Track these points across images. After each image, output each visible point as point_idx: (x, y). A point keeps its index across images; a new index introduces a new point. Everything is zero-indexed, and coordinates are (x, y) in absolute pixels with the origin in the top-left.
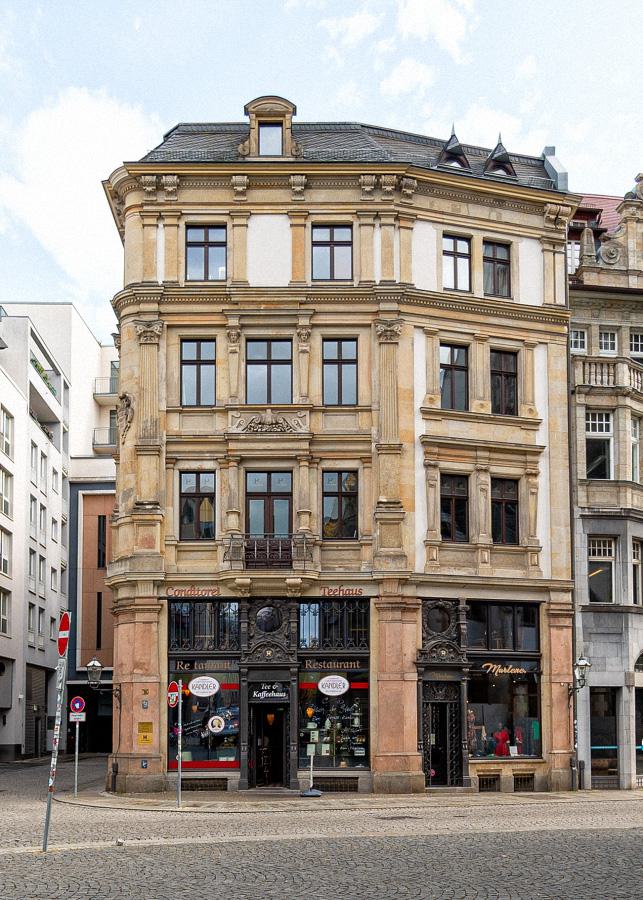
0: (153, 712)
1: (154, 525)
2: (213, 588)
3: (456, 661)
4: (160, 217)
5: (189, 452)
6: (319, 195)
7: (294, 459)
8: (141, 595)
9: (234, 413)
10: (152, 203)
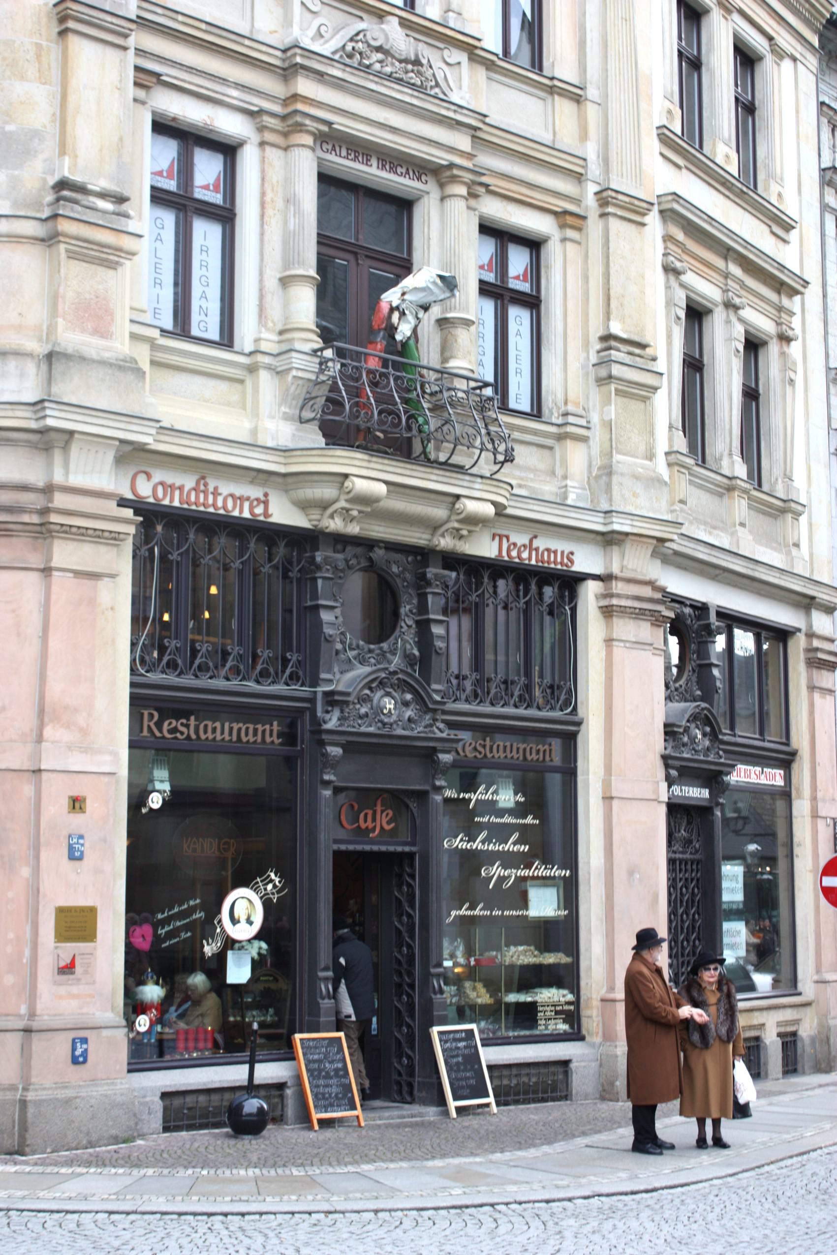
0: (98, 871)
1: (112, 266)
2: (255, 492)
3: (418, 730)
5: (190, 69)
8: (76, 480)
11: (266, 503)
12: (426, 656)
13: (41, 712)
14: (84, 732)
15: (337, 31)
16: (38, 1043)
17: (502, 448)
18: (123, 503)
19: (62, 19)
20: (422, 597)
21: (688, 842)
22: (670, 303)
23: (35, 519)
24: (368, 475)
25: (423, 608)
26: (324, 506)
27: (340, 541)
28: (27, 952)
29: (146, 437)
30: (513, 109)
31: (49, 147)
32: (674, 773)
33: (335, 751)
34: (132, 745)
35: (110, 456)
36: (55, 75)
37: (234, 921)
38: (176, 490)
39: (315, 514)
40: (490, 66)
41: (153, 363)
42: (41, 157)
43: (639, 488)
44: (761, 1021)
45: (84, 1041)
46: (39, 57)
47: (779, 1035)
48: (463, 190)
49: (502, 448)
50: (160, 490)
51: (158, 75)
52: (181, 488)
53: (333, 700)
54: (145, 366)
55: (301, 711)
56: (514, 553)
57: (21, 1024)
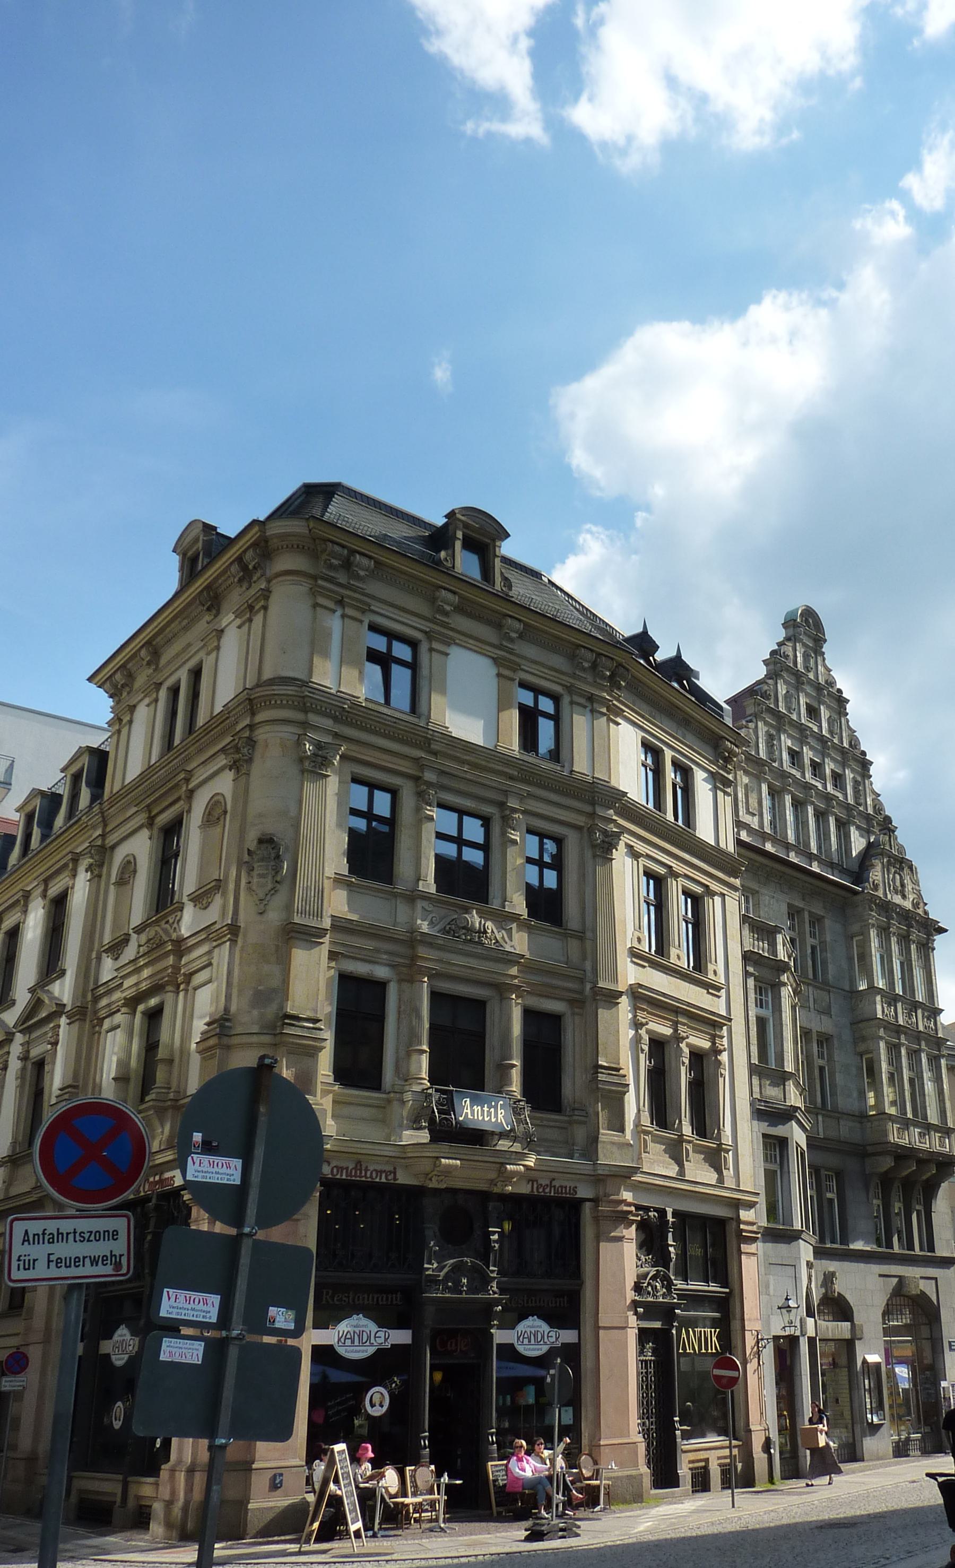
11: (395, 1173)
15: (441, 919)
43: (615, 1149)
44: (706, 1456)
45: (281, 1475)
46: (277, 951)
47: (720, 1465)
50: (335, 1170)
52: (347, 1169)
56: (541, 1190)
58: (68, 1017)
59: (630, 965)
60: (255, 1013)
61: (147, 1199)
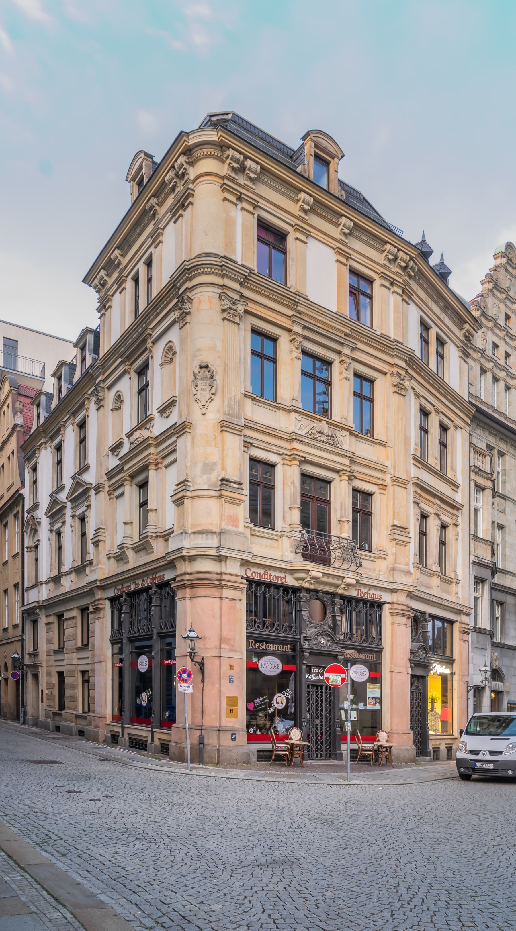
1: (238, 505)
2: (282, 575)
4: (239, 199)
6: (357, 245)
7: (337, 471)
8: (229, 571)
9: (297, 415)
10: (233, 180)
11: (285, 578)
12: (335, 627)
13: (221, 640)
14: (233, 646)
16: (222, 734)
17: (358, 562)
18: (243, 578)
19: (222, 427)
20: (334, 608)
21: (417, 687)
22: (415, 514)
23: (218, 583)
24: (316, 570)
25: (334, 611)
26: (303, 579)
27: (308, 590)
28: (218, 709)
29: (248, 557)
30: (363, 449)
31: (219, 468)
32: (413, 665)
33: (307, 654)
34: (247, 651)
35: (239, 563)
36: (220, 445)
37: (277, 703)
38: (258, 574)
39: (300, 582)
40: (356, 436)
41: (251, 535)
42: (216, 471)
45: (235, 734)
46: (215, 439)
48: (347, 478)
49: (358, 562)
51: (251, 443)
53: (306, 639)
54: (249, 536)
55: (297, 642)
57: (217, 729)
58: (95, 490)
59: (412, 465)
60: (205, 477)
61: (150, 588)
